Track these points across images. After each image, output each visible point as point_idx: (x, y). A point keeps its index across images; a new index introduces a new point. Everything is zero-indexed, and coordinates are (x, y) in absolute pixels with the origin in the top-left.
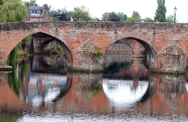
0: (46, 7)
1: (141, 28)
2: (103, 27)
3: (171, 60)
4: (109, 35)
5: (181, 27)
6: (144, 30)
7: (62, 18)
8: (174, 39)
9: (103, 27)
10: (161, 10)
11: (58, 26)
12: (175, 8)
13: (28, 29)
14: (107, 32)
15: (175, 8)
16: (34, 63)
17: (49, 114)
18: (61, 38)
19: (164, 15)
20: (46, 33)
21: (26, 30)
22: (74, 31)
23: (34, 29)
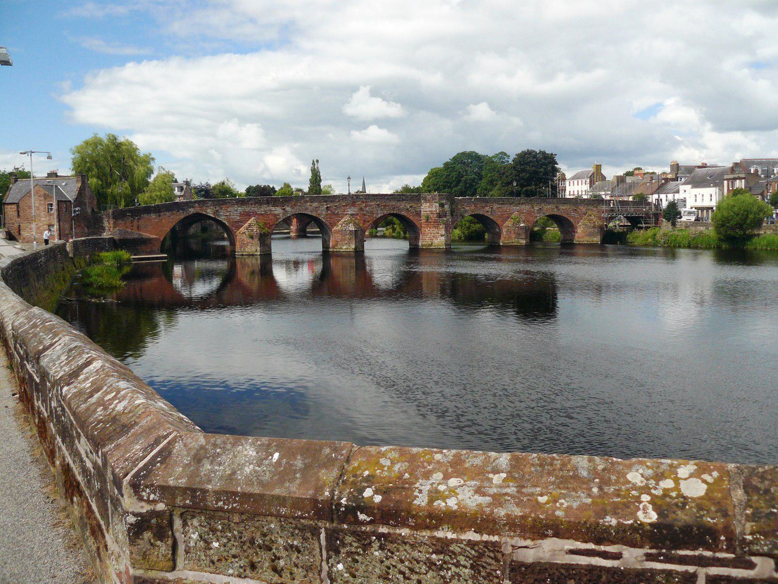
0: (187, 183)
1: (312, 202)
2: (268, 203)
3: (348, 236)
4: (276, 212)
5: (357, 198)
6: (315, 204)
7: (206, 192)
8: (349, 213)
9: (268, 203)
10: (316, 178)
11: (217, 204)
12: (349, 178)
13: (183, 210)
14: (273, 209)
15: (349, 178)
16: (178, 249)
17: (326, 297)
18: (222, 218)
19: (320, 185)
20: (204, 213)
21: (181, 211)
22: (236, 209)
23: (190, 210)
